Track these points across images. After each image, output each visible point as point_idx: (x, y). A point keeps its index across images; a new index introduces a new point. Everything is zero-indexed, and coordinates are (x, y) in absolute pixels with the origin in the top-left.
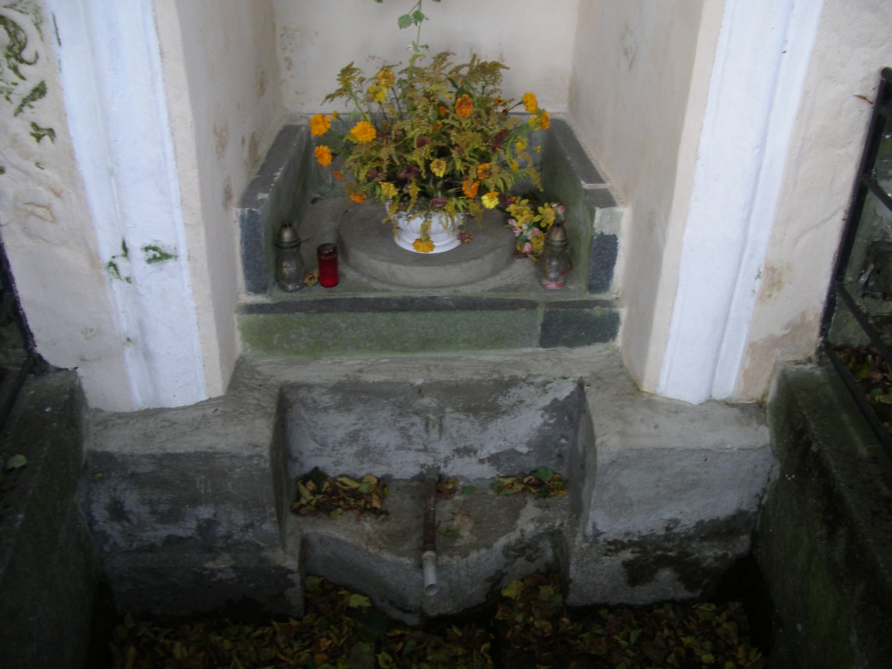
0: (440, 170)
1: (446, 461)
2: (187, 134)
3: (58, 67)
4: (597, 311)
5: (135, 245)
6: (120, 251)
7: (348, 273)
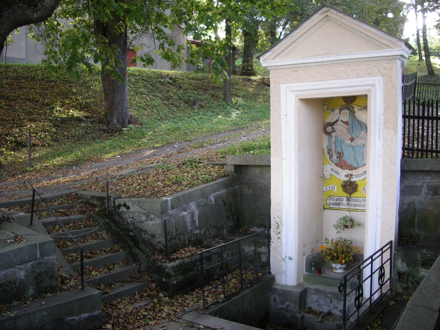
1: (332, 309)
2: (297, 242)
3: (282, 230)
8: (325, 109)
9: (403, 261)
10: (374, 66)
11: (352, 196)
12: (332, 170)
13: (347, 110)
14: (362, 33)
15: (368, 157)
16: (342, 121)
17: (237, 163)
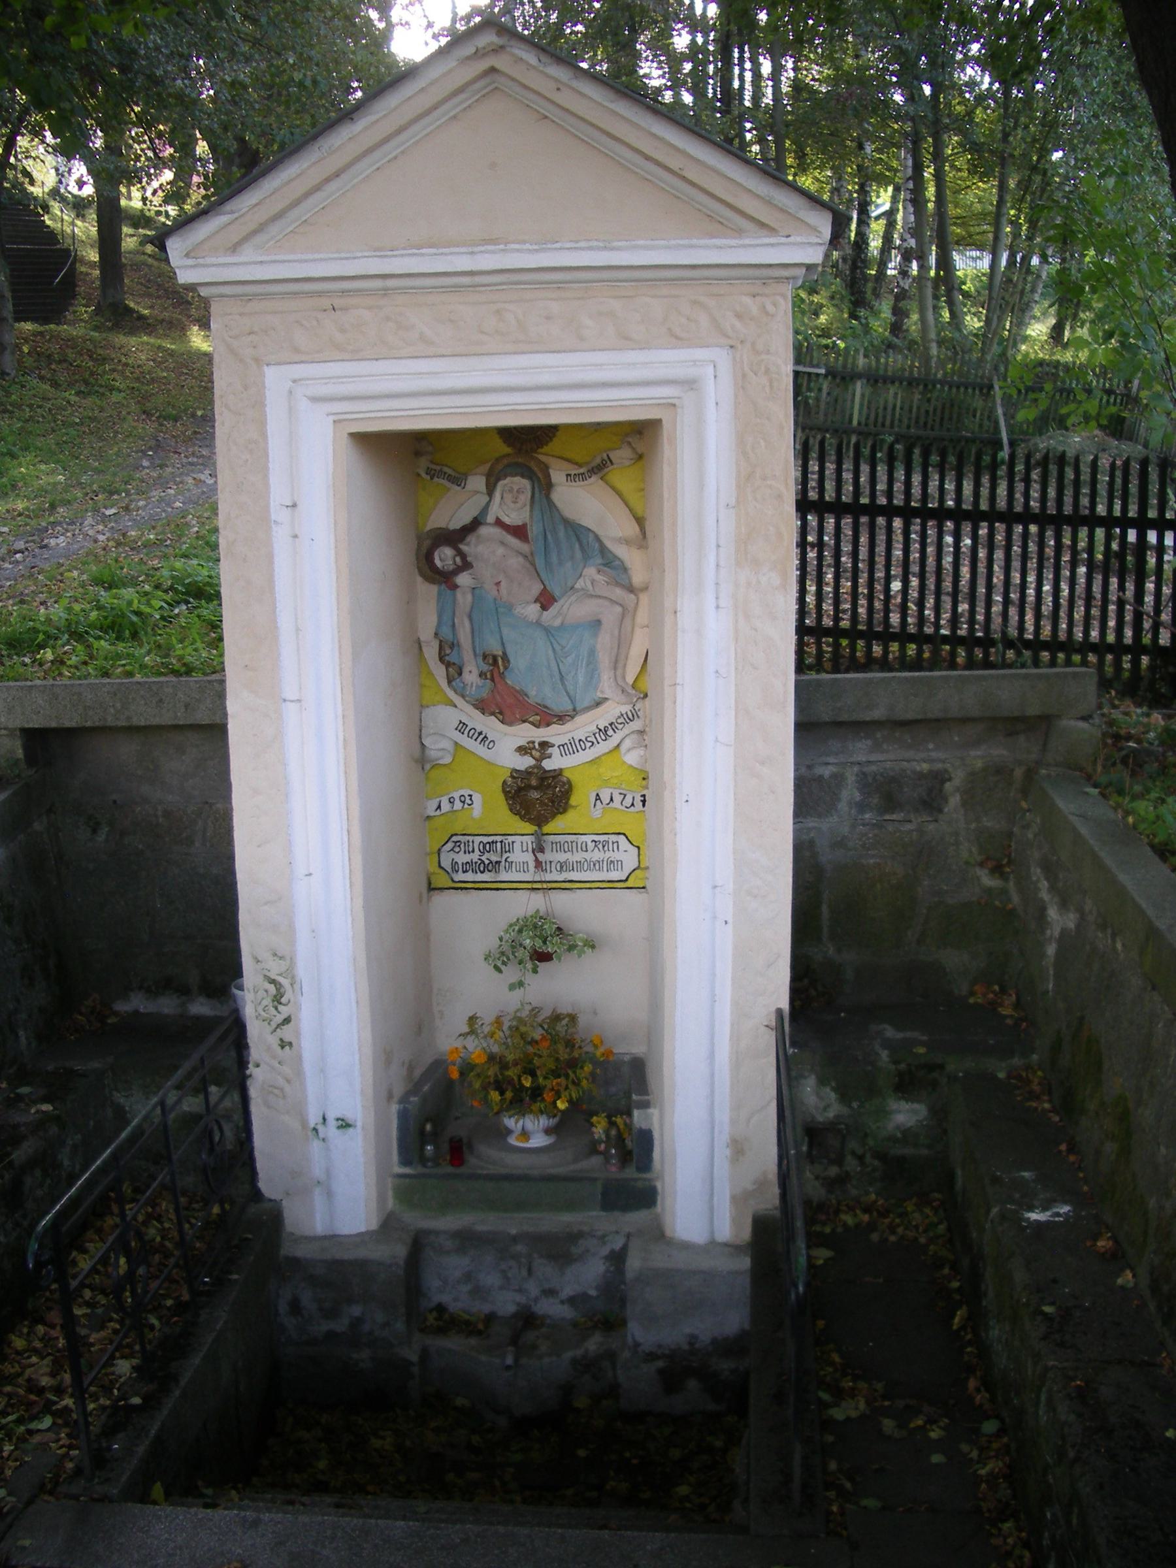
0: (527, 1083)
1: (536, 1300)
2: (368, 1050)
3: (299, 1008)
4: (640, 1184)
5: (331, 1117)
6: (321, 1120)
7: (472, 1161)
8: (424, 475)
9: (822, 1082)
10: (695, 302)
11: (547, 829)
12: (462, 727)
13: (523, 476)
14: (648, 158)
15: (667, 682)
16: (499, 523)
17: (36, 723)
